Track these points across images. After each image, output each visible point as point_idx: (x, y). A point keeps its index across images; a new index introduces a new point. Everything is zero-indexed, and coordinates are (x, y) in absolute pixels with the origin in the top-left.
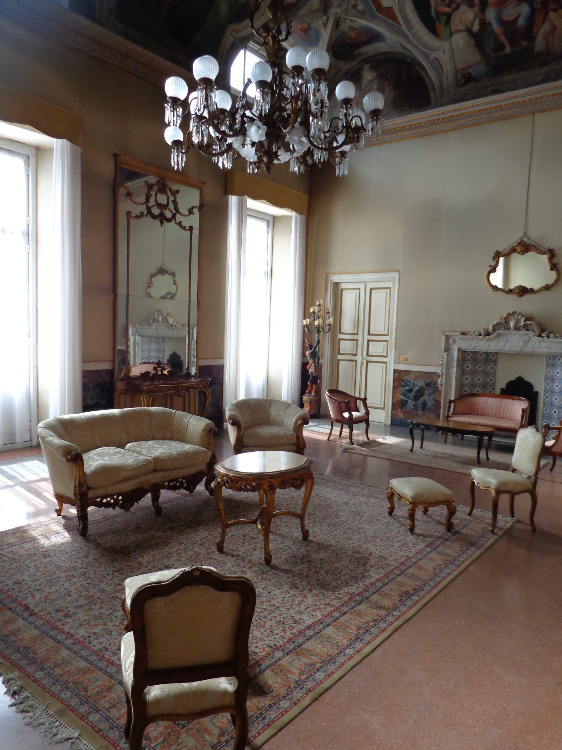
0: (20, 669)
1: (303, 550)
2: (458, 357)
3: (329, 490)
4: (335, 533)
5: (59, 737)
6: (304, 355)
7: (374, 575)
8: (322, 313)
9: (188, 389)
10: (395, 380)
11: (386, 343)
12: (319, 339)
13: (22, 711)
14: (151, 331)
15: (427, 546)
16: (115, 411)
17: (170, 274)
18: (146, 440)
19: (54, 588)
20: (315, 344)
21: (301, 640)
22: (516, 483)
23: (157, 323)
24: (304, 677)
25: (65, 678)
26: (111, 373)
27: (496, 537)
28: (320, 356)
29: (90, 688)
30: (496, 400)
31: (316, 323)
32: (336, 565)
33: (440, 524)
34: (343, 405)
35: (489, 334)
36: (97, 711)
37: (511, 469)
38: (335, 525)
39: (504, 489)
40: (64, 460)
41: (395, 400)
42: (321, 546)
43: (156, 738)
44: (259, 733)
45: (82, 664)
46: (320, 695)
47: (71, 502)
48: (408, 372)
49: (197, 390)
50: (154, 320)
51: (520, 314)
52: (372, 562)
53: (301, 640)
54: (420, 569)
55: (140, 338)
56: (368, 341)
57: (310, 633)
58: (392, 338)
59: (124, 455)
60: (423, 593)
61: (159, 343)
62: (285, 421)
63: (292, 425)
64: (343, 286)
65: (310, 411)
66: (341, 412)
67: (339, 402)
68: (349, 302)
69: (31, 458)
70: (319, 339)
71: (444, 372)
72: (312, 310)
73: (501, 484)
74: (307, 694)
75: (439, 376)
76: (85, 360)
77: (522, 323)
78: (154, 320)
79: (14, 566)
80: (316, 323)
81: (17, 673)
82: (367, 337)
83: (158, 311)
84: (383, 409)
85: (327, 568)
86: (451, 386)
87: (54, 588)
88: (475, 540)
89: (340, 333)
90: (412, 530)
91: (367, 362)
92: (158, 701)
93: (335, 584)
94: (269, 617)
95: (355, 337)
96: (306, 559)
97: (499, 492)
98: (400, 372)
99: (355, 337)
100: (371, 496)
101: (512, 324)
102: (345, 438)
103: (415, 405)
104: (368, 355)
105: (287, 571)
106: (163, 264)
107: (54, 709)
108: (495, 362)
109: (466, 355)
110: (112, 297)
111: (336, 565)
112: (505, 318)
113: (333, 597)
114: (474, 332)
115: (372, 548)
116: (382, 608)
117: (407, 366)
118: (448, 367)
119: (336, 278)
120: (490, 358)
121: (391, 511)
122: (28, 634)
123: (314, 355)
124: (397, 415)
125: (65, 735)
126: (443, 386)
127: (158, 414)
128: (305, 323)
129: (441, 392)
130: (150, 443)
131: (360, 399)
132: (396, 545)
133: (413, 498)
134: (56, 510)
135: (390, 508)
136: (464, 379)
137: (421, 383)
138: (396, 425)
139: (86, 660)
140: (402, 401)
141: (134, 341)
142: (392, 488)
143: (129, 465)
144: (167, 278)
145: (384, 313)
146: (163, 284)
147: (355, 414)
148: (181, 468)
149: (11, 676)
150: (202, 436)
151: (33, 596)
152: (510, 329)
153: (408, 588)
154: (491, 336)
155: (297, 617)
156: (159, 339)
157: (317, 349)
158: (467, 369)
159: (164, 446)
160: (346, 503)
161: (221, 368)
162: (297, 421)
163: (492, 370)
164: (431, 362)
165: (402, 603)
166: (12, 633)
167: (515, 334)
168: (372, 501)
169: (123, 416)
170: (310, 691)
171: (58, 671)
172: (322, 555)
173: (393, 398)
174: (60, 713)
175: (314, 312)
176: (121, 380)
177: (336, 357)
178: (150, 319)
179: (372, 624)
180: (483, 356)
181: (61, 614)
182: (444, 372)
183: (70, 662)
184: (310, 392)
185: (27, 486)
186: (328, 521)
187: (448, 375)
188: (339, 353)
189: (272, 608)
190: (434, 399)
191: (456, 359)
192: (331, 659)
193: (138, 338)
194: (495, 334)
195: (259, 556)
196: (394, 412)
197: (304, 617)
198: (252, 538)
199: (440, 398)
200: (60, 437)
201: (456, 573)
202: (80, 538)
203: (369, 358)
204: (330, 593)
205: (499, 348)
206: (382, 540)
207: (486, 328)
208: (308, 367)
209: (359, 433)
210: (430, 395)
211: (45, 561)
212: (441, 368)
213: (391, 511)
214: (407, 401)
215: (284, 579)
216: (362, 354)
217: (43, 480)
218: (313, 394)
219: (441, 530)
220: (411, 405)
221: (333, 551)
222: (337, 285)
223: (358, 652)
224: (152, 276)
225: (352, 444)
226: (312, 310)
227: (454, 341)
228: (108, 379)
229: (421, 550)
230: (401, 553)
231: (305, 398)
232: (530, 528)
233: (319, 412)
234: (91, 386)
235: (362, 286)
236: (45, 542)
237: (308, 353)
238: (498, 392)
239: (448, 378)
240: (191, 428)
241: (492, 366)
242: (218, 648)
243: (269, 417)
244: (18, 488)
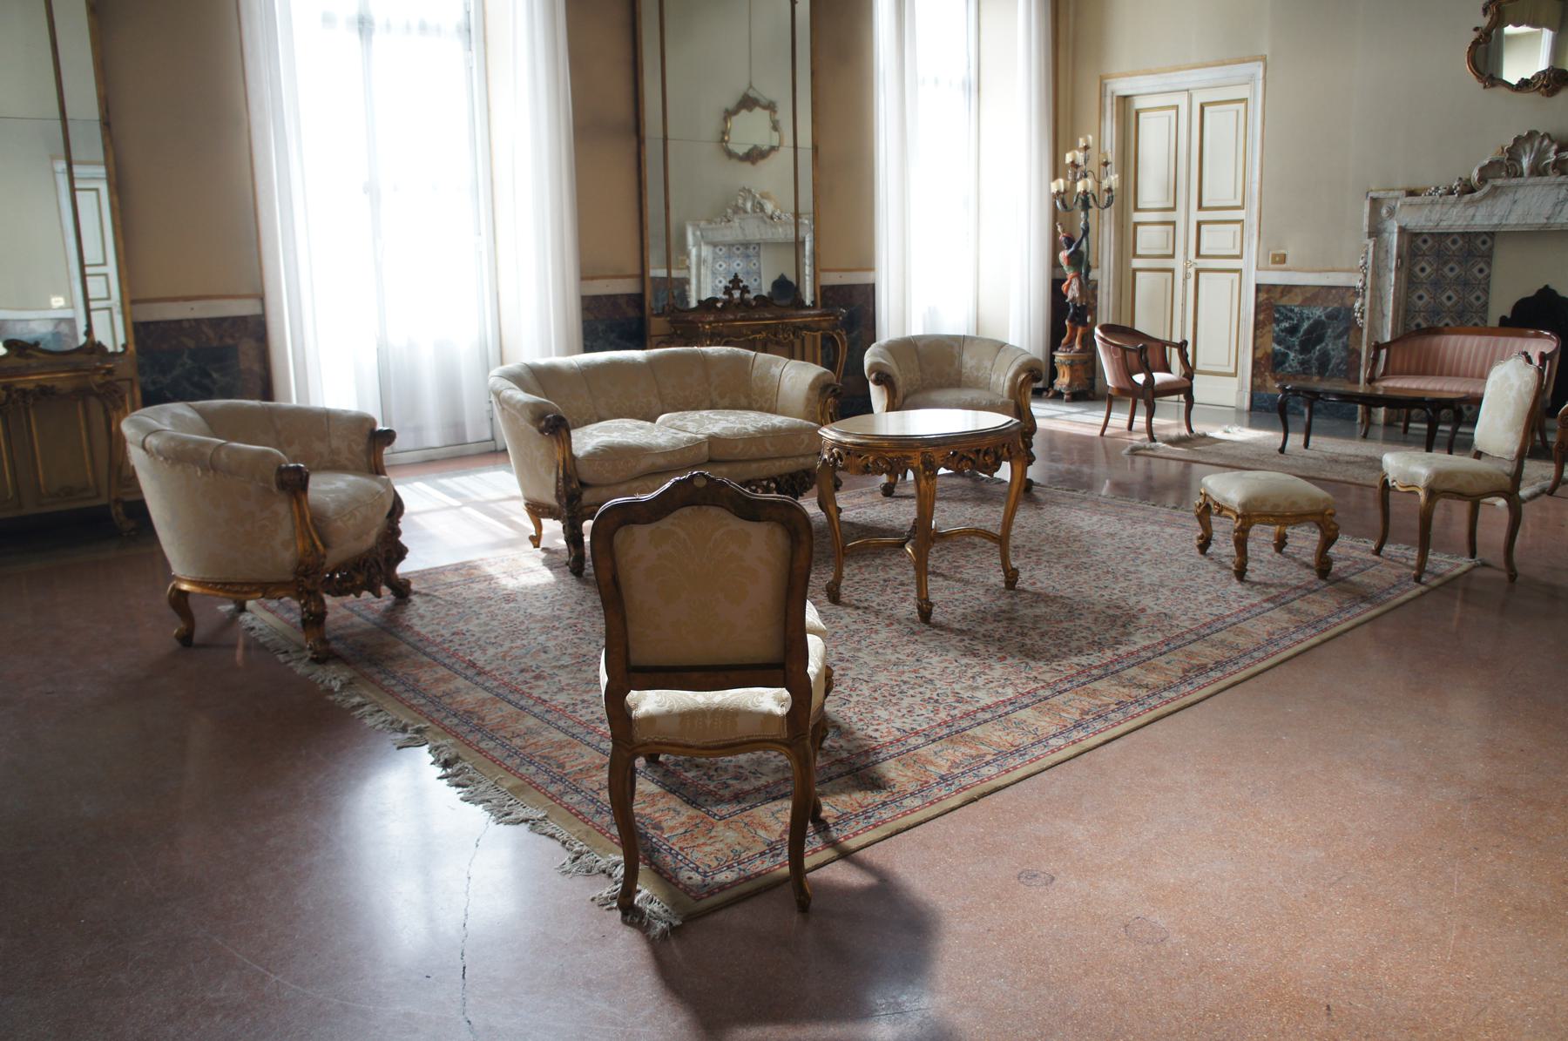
0: (457, 736)
1: (1003, 603)
2: (1399, 247)
3: (1081, 514)
4: (1076, 578)
5: (512, 817)
6: (1055, 264)
7: (1140, 640)
8: (1093, 165)
9: (797, 329)
10: (1258, 308)
11: (1238, 226)
12: (1086, 224)
13: (458, 785)
14: (732, 232)
15: (1267, 601)
16: (638, 355)
17: (765, 108)
18: (696, 408)
19: (519, 642)
20: (1078, 235)
21: (965, 724)
22: (1477, 475)
23: (742, 215)
24: (956, 771)
25: (528, 750)
26: (638, 300)
27: (1423, 588)
28: (1092, 263)
29: (568, 765)
30: (1485, 339)
31: (1080, 187)
32: (1065, 625)
33: (1308, 566)
34: (1133, 358)
35: (1472, 190)
36: (577, 791)
37: (1473, 452)
38: (1081, 567)
39: (1446, 486)
40: (534, 430)
41: (1259, 355)
42: (1039, 597)
43: (672, 829)
44: (856, 834)
45: (560, 736)
46: (984, 795)
47: (552, 514)
48: (1287, 289)
49: (819, 334)
50: (738, 210)
51: (1547, 135)
52: (1143, 621)
53: (965, 724)
54: (1242, 632)
55: (710, 249)
56: (1199, 224)
57: (981, 716)
58: (1250, 215)
59: (650, 430)
60: (1235, 668)
61: (748, 256)
62: (994, 378)
63: (1007, 384)
64: (1139, 103)
65: (1070, 385)
66: (1129, 374)
67: (1124, 350)
68: (1155, 141)
69: (496, 466)
70: (1086, 224)
71: (1369, 284)
72: (1069, 158)
73: (1439, 476)
74: (957, 792)
75: (1357, 294)
76: (586, 273)
77: (1552, 157)
78: (738, 210)
79: (454, 611)
80: (1080, 187)
81: (451, 740)
82: (1197, 215)
83: (744, 189)
84: (1235, 375)
85: (1045, 627)
86: (1384, 315)
87: (519, 642)
88: (1376, 591)
89: (1136, 209)
90: (1241, 573)
91: (1198, 272)
92: (651, 719)
93: (1054, 651)
94: (911, 692)
95: (1169, 216)
96: (1007, 617)
97: (1433, 493)
98: (1271, 288)
99: (1169, 216)
100: (1169, 524)
101: (1526, 162)
102: (1139, 432)
103: (1302, 363)
104: (1198, 255)
105: (961, 632)
106: (751, 86)
107: (508, 785)
108: (1488, 257)
109: (1419, 242)
110: (634, 143)
111: (1065, 625)
112: (1509, 150)
113: (1046, 668)
114: (1437, 188)
115: (1148, 601)
116: (1140, 686)
117: (1285, 274)
118: (1377, 274)
119: (1121, 86)
120: (1477, 247)
121: (1204, 544)
122: (471, 696)
123: (1078, 260)
124: (1263, 386)
125: (522, 816)
126: (1367, 316)
127: (721, 359)
128: (1054, 189)
129: (1361, 329)
130: (705, 413)
131: (1172, 345)
132: (1202, 598)
133: (1244, 505)
134: (532, 538)
135: (1201, 537)
136: (1415, 297)
137: (1318, 312)
138: (1262, 408)
139: (566, 733)
140: (1276, 353)
141: (699, 256)
142: (1206, 495)
143: (659, 446)
144: (760, 117)
145: (1233, 163)
146: (751, 130)
147: (1159, 377)
148: (763, 459)
149: (440, 742)
150: (808, 400)
151: (484, 651)
152: (1521, 175)
153: (1204, 661)
154: (1477, 195)
155: (965, 695)
156: (747, 248)
157: (1083, 247)
158: (1423, 275)
159: (732, 418)
160: (1112, 535)
161: (869, 291)
162: (1016, 375)
163: (1480, 276)
164: (1338, 263)
165: (1184, 680)
166: (445, 694)
167: (1534, 185)
168: (1169, 530)
169: (652, 363)
170: (964, 788)
171: (518, 742)
172: (1041, 609)
173: (1255, 349)
174: (515, 791)
175: (1074, 165)
176: (658, 315)
177: (1129, 263)
178: (728, 209)
179: (1113, 707)
180: (1460, 242)
181: (528, 676)
182: (1369, 284)
183: (539, 734)
184: (1070, 344)
185: (483, 506)
186: (1067, 561)
187: (1377, 290)
188: (1135, 255)
189: (919, 681)
190: (1346, 347)
191: (1394, 251)
192: (1018, 750)
193: (706, 251)
194: (1487, 188)
195: (909, 608)
196: (1258, 381)
197: (979, 694)
198: (902, 584)
199: (1360, 342)
200: (527, 390)
201: (1315, 640)
202: (571, 578)
203: (1202, 263)
204: (1041, 664)
205: (1495, 221)
206: (1173, 590)
207: (1465, 177)
208: (1064, 287)
209: (1168, 421)
210: (1340, 336)
211: (507, 607)
212: (1361, 276)
213: (1204, 544)
214: (1286, 355)
215: (953, 642)
216: (1186, 254)
217: (513, 498)
218: (1077, 347)
219: (1309, 576)
220: (1295, 364)
221: (1064, 605)
222: (1125, 100)
223: (1074, 742)
224: (729, 114)
225: (1152, 439)
226: (1069, 158)
227: (1391, 213)
228: (632, 313)
229: (1253, 606)
230: (1207, 610)
231: (1060, 356)
232: (1504, 575)
233: (1093, 386)
234: (601, 328)
235: (1182, 101)
236: (510, 584)
237: (1063, 255)
238: (1493, 321)
239: (1378, 297)
240: (786, 384)
241: (1482, 265)
242: (751, 635)
243: (960, 373)
244: (468, 510)
